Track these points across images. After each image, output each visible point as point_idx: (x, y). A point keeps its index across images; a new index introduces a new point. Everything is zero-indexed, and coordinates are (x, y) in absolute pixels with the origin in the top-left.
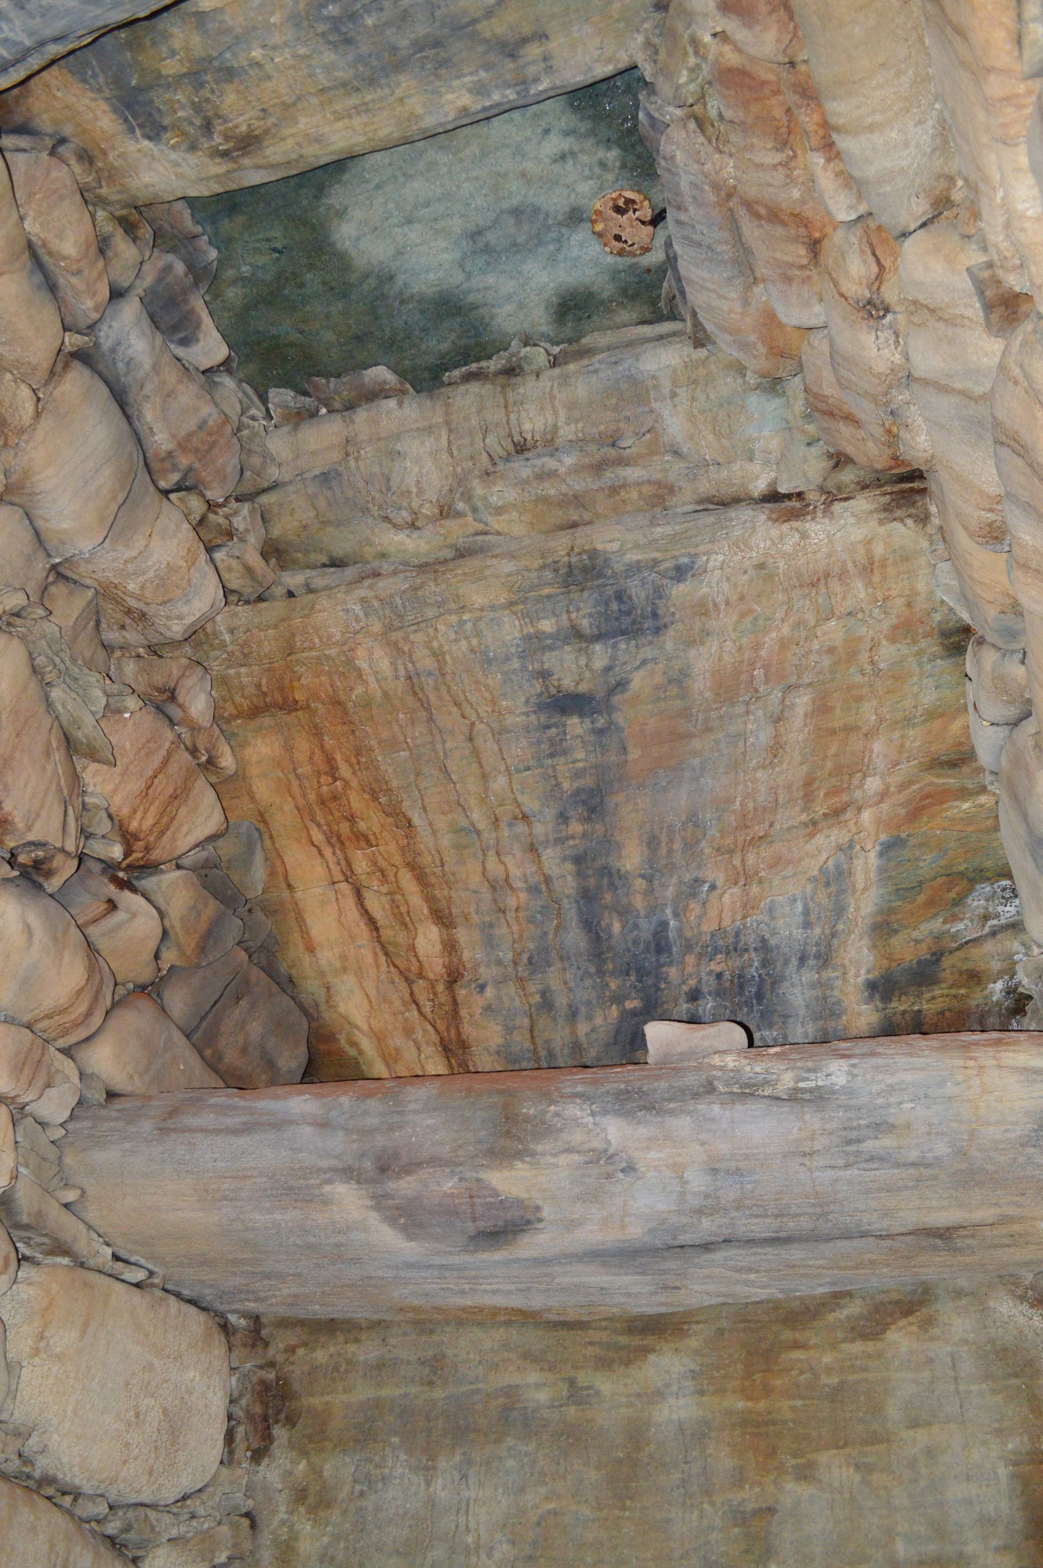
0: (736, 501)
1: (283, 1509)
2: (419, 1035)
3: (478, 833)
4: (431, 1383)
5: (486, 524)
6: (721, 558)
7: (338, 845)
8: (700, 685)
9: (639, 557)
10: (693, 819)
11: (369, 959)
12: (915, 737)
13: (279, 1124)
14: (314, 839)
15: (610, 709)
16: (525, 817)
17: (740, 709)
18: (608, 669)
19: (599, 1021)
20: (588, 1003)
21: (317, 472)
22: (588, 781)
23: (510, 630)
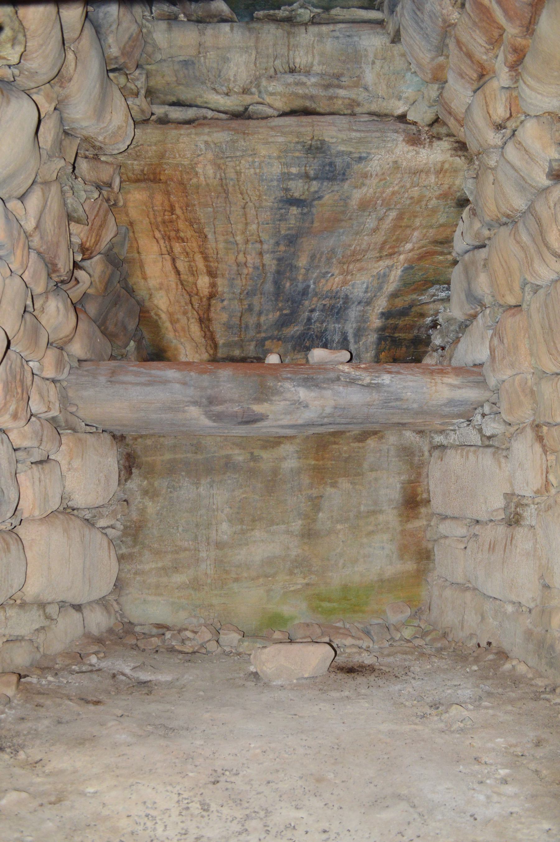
0: (386, 115)
1: (139, 497)
2: (190, 315)
3: (237, 244)
4: (196, 453)
5: (263, 99)
6: (380, 156)
7: (167, 240)
8: (354, 203)
9: (344, 149)
10: (333, 251)
11: (174, 286)
12: (431, 233)
13: (165, 382)
14: (156, 236)
15: (311, 206)
16: (261, 242)
17: (366, 213)
18: (316, 192)
19: (270, 316)
20: (268, 311)
21: (181, 58)
22: (293, 232)
23: (276, 169)
